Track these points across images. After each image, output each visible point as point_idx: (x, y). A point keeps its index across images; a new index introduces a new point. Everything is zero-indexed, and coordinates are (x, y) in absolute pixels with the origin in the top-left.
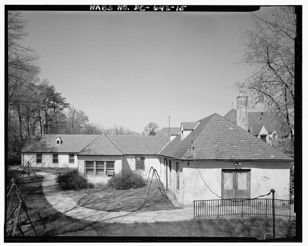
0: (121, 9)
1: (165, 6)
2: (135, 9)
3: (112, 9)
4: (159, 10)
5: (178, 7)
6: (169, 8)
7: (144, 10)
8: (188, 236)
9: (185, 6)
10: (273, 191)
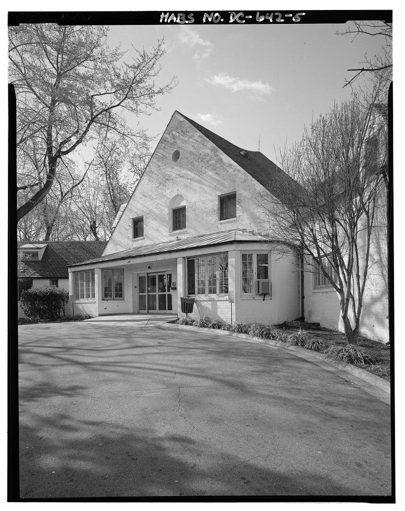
0: (210, 20)
1: (274, 12)
2: (230, 21)
3: (193, 21)
4: (266, 22)
5: (258, 13)
6: (281, 19)
7: (244, 21)
8: (391, 482)
9: (304, 14)
10: (264, 300)
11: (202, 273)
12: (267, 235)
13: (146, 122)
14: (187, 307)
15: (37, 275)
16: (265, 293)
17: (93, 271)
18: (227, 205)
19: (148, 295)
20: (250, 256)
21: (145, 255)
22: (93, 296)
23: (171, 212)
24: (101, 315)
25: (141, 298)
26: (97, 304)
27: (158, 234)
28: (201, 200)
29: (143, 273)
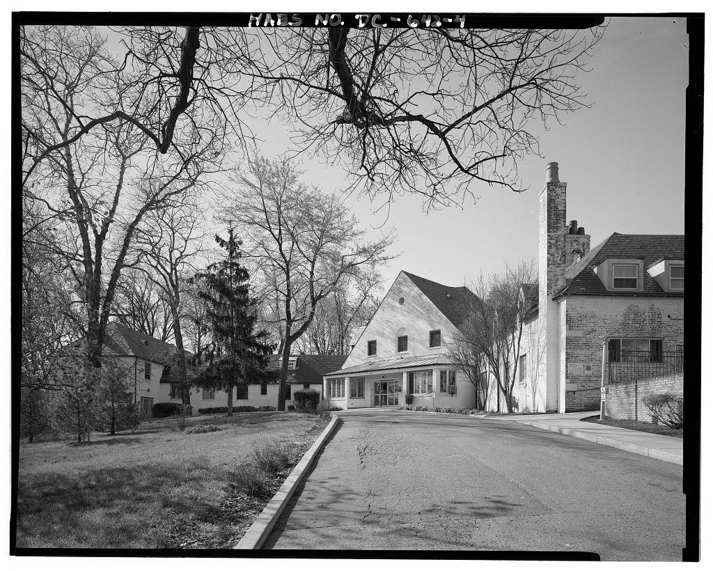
11: (419, 381)
12: (383, 428)
13: (388, 274)
14: (410, 400)
15: (294, 381)
16: (453, 392)
17: (344, 379)
18: (435, 338)
19: (382, 396)
20: (445, 372)
21: (382, 370)
22: (343, 396)
23: (397, 339)
24: (348, 408)
25: (376, 397)
26: (346, 401)
27: (388, 354)
28: (419, 329)
29: (378, 381)
